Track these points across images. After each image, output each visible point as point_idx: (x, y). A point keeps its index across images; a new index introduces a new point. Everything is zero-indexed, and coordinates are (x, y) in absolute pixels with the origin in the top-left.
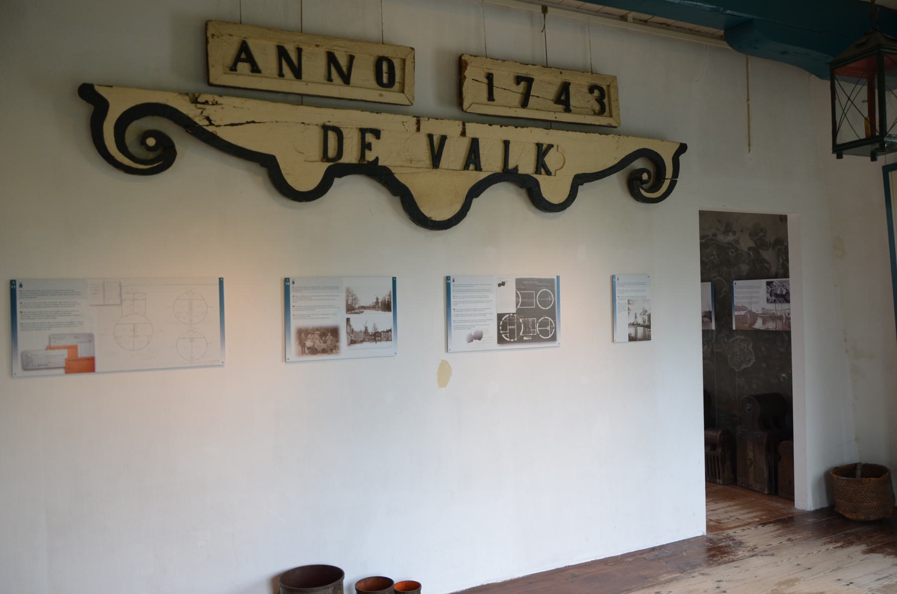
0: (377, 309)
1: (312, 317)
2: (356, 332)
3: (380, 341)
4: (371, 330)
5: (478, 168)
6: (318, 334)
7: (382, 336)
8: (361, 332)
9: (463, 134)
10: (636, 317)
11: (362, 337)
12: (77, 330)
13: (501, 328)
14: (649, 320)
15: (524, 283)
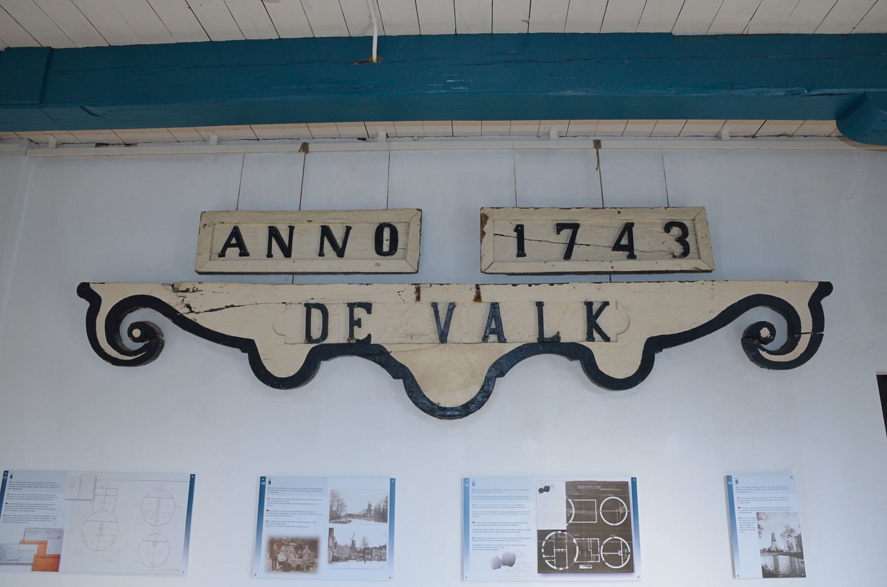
0: (368, 518)
1: (288, 524)
2: (340, 546)
3: (371, 560)
4: (359, 545)
5: (502, 339)
6: (293, 546)
7: (374, 554)
8: (346, 546)
9: (478, 298)
10: (773, 540)
11: (347, 552)
12: (50, 525)
13: (543, 550)
14: (800, 544)
15: (579, 487)
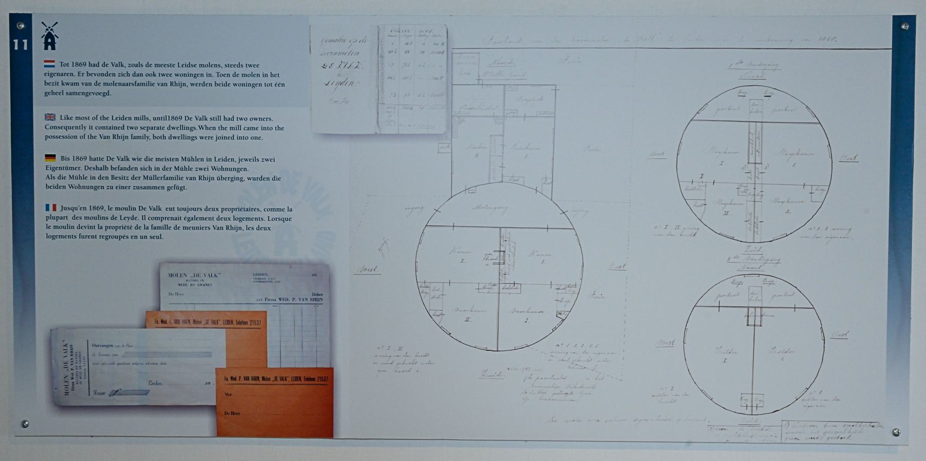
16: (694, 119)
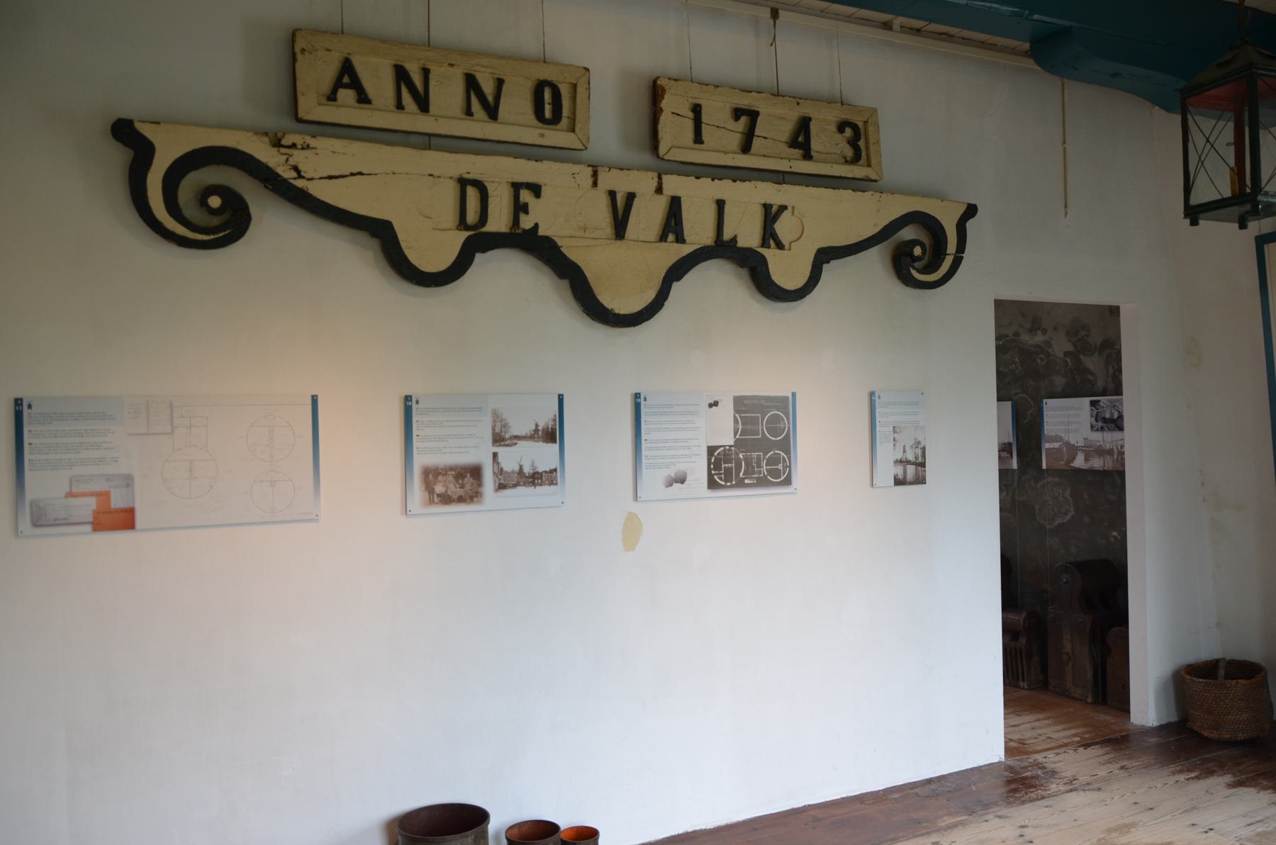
0: (536, 440)
1: (444, 450)
2: (506, 472)
3: (541, 485)
4: (527, 470)
5: (680, 239)
6: (452, 475)
7: (544, 479)
8: (513, 472)
9: (659, 190)
10: (904, 451)
11: (515, 479)
12: (110, 469)
13: (712, 466)
14: (924, 456)
15: (746, 402)
16: (1207, 136)
